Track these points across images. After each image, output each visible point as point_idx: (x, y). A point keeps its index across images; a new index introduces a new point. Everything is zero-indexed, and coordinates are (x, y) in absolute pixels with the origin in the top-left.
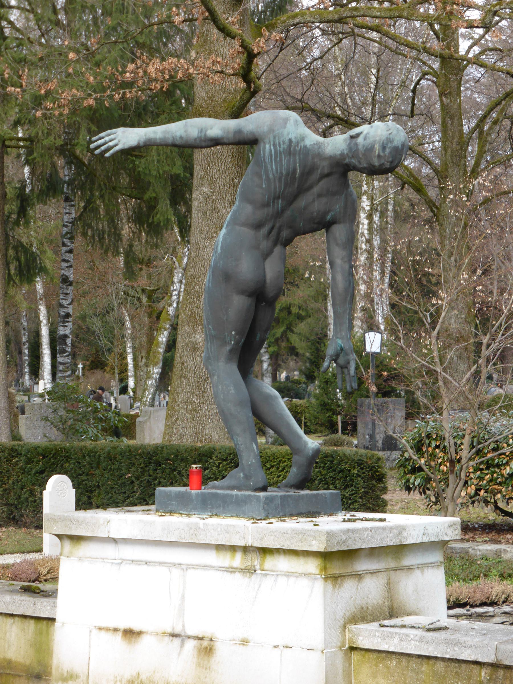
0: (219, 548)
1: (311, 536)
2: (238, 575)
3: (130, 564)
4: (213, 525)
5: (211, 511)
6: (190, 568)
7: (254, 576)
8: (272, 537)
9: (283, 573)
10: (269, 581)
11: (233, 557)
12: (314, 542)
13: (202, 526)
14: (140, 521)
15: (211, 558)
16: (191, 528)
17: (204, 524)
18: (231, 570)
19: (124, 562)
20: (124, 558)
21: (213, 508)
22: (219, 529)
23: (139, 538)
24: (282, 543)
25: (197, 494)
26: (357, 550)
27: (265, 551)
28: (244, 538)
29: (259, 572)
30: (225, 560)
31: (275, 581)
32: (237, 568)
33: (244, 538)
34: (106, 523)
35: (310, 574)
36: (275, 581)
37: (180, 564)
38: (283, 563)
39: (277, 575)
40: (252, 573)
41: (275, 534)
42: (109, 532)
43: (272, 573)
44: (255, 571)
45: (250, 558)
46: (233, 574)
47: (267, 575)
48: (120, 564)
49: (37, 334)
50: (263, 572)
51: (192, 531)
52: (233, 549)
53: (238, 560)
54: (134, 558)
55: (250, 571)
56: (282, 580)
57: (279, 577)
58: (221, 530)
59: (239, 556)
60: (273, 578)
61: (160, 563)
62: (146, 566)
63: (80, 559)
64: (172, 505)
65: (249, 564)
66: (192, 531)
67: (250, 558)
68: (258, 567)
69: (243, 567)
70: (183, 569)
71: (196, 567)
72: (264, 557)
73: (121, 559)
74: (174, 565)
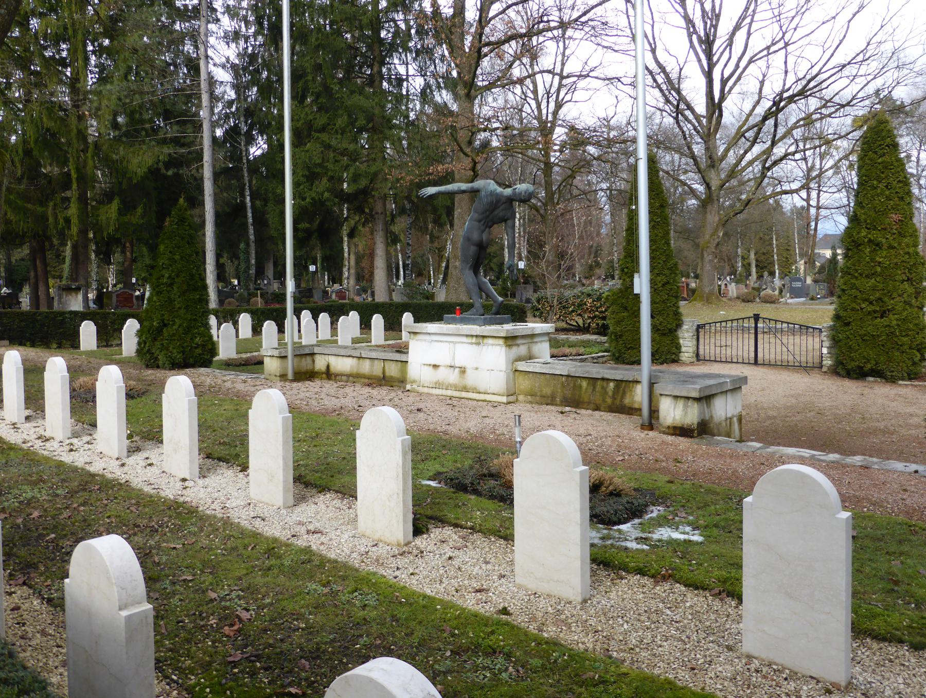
0: (467, 336)
10: (485, 347)
15: (464, 339)
27: (484, 337)
30: (469, 340)
38: (490, 341)
52: (472, 336)
53: (474, 340)
55: (478, 344)
56: (490, 347)
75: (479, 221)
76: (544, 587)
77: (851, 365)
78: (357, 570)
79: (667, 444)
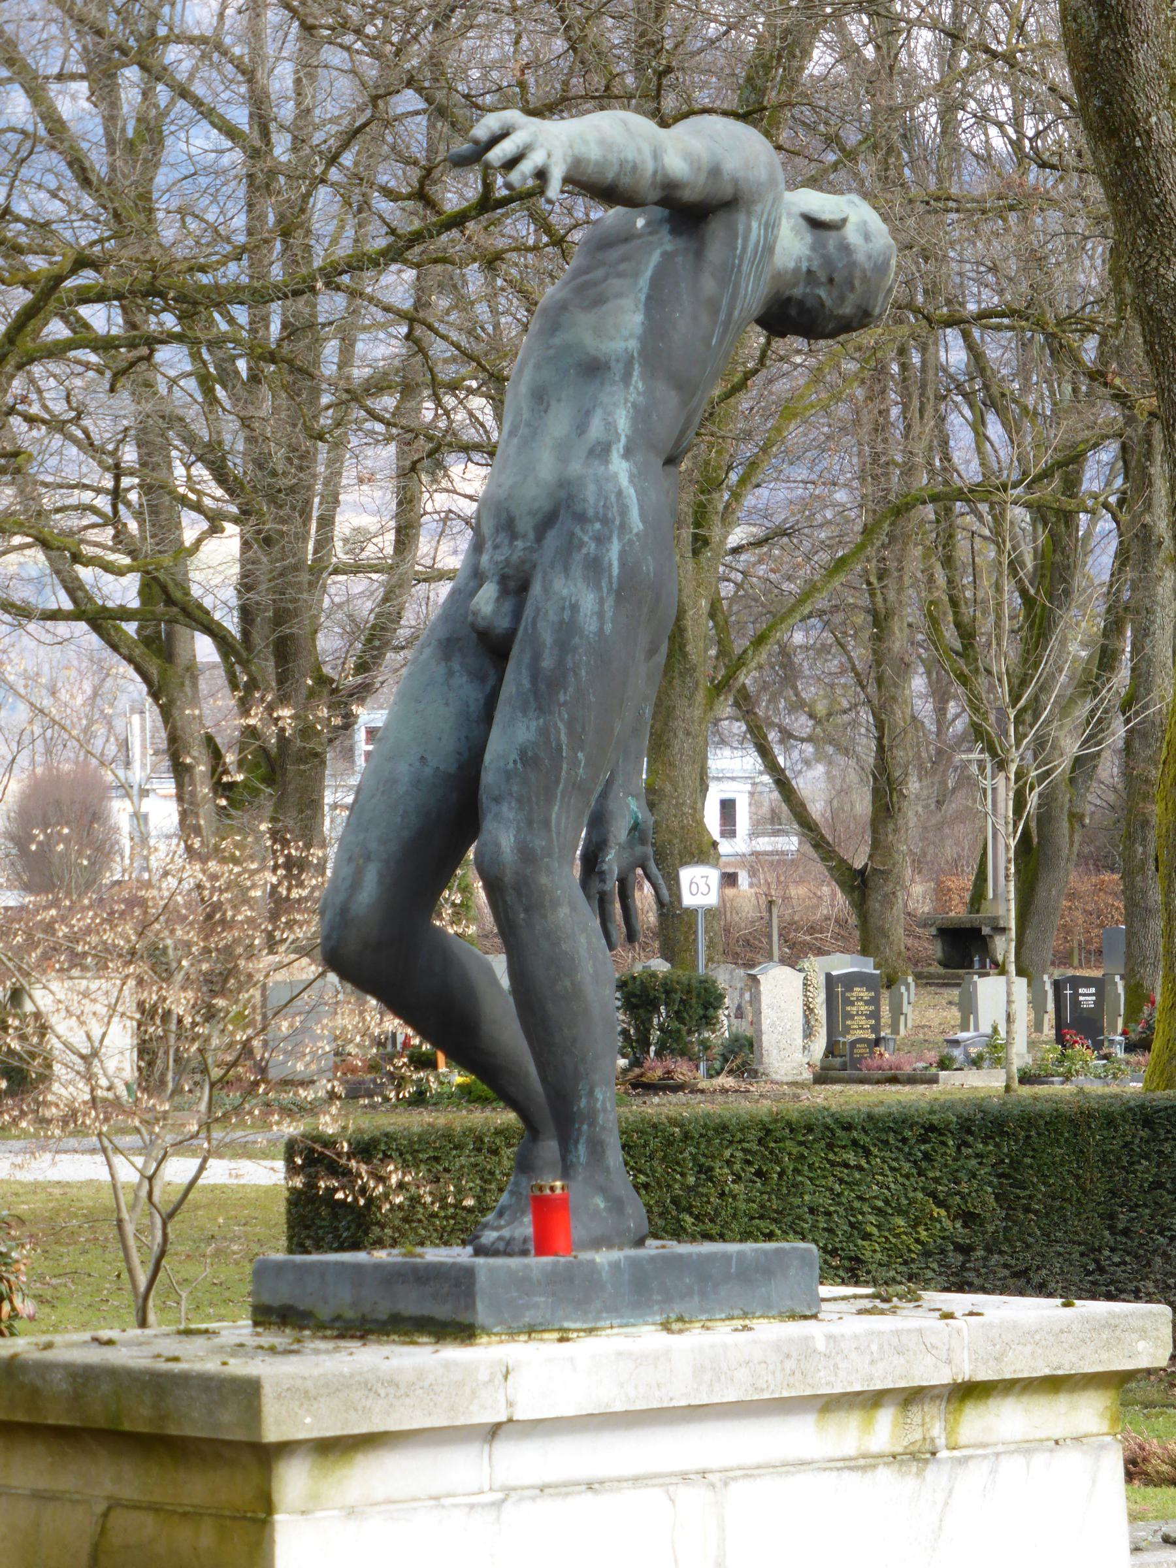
0: (831, 1404)
1: (1134, 1330)
2: (884, 1475)
3: (533, 1498)
4: (856, 1337)
5: (662, 1311)
6: (735, 1479)
7: (931, 1471)
8: (1028, 1349)
9: (1012, 1447)
10: (975, 1475)
11: (869, 1423)
12: (1141, 1345)
13: (821, 1345)
14: (619, 1354)
15: (802, 1436)
16: (788, 1356)
17: (830, 1337)
18: (862, 1462)
19: (514, 1496)
20: (512, 1483)
21: (668, 1299)
22: (874, 1347)
23: (618, 1407)
24: (1055, 1361)
25: (615, 1266)
26: (386, 1434)
27: (969, 1392)
28: (949, 1362)
29: (943, 1454)
30: (847, 1435)
31: (993, 1471)
32: (881, 1456)
33: (949, 1362)
34: (500, 1377)
35: (1085, 1436)
36: (993, 1471)
37: (703, 1473)
38: (1007, 1419)
39: (998, 1455)
40: (926, 1461)
41: (1037, 1337)
42: (510, 1404)
43: (980, 1452)
44: (934, 1454)
45: (917, 1419)
46: (869, 1474)
47: (967, 1459)
48: (498, 1505)
49: (986, 844)
50: (956, 1453)
51: (790, 1365)
52: (874, 1400)
53: (884, 1431)
54: (549, 1478)
55: (919, 1456)
56: (1012, 1465)
57: (1003, 1458)
58: (881, 1347)
59: (886, 1417)
60: (986, 1465)
61: (636, 1479)
62: (589, 1495)
63: (352, 1512)
64: (536, 1306)
65: (917, 1435)
66: (790, 1365)
67: (917, 1419)
68: (941, 1442)
69: (900, 1450)
70: (713, 1486)
71: (750, 1472)
72: (959, 1410)
73: (502, 1489)
74: (684, 1477)
75: (642, 1120)
76: (969, 1099)
77: (290, 1251)
78: (207, 613)
79: (711, 940)
